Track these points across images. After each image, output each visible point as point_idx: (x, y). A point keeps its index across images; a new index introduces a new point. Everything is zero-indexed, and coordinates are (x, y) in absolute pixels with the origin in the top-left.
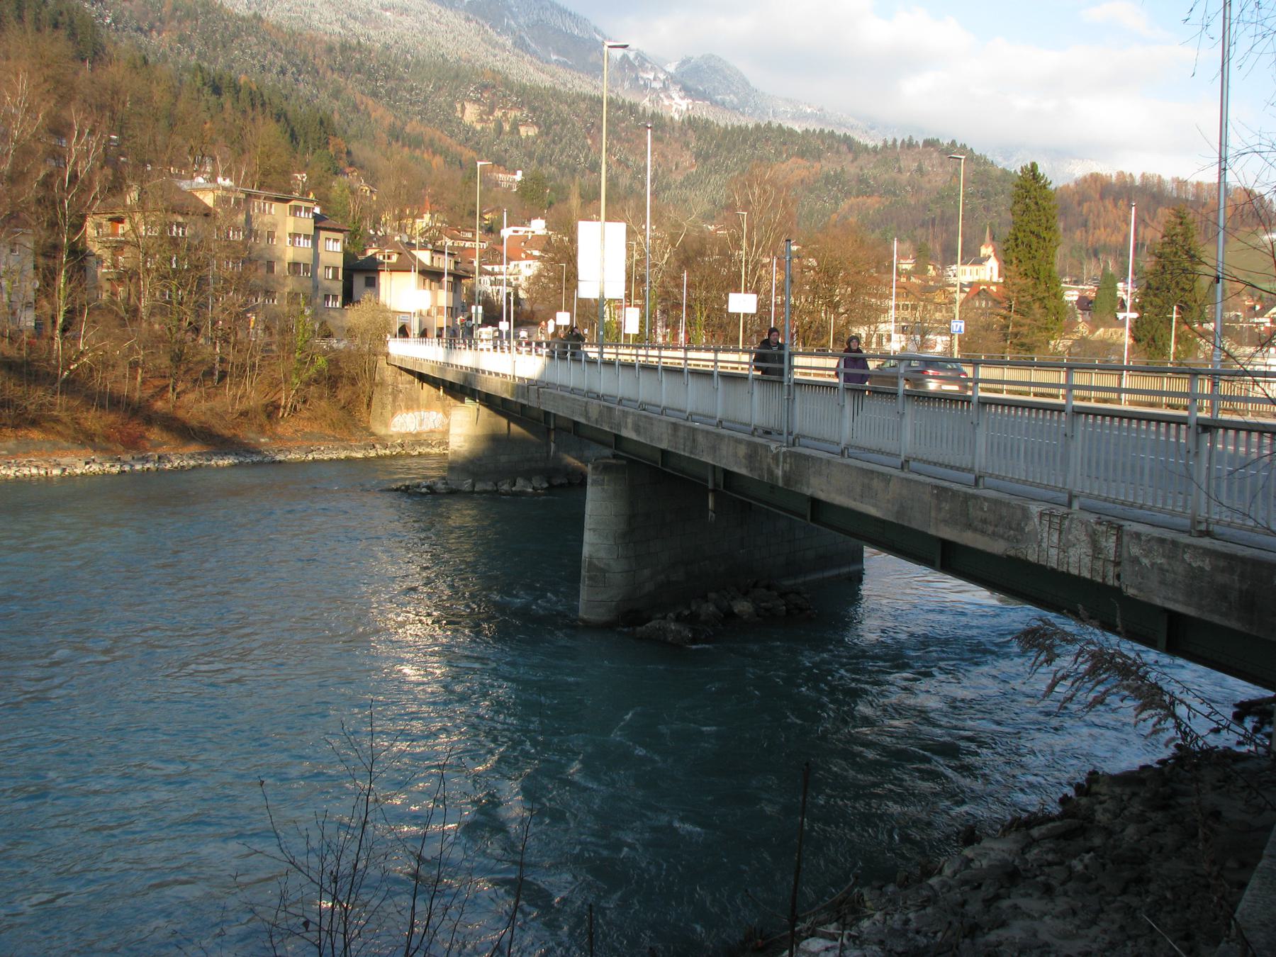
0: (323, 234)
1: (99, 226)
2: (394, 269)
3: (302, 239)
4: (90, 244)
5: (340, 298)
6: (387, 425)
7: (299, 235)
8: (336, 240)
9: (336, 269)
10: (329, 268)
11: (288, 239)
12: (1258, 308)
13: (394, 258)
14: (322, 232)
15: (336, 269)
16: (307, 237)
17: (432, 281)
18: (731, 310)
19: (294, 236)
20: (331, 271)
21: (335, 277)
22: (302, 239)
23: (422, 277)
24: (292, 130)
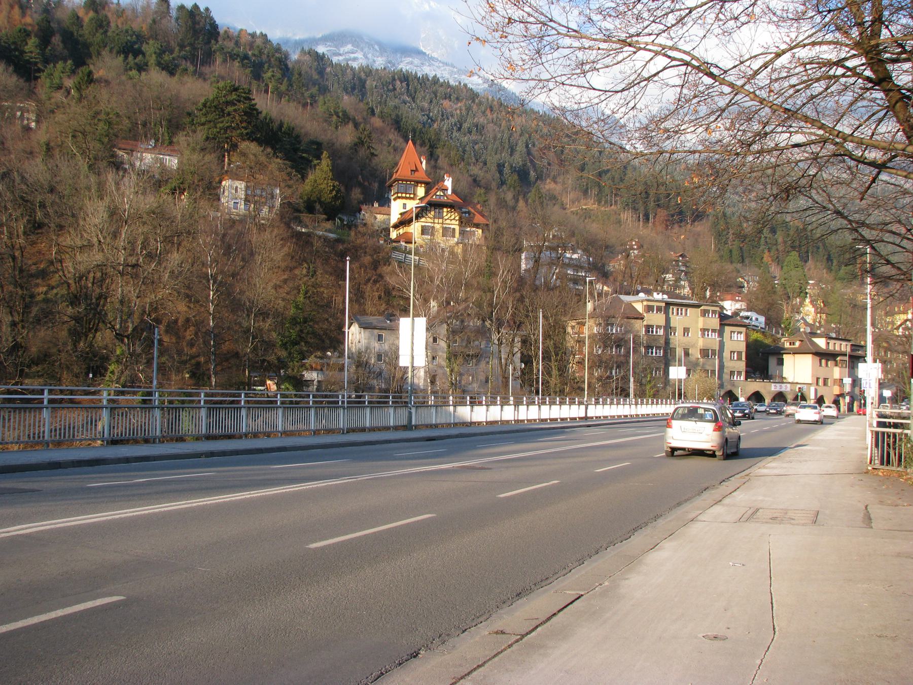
0: (728, 329)
1: (573, 327)
2: (796, 352)
3: (710, 333)
4: (108, 307)
5: (743, 374)
6: (131, 152)
7: (708, 330)
8: (741, 333)
9: (739, 353)
10: (734, 352)
11: (700, 333)
12: (885, 345)
13: (797, 344)
14: (726, 328)
15: (739, 353)
16: (714, 331)
17: (827, 361)
18: (860, 364)
19: (704, 330)
20: (736, 354)
21: (739, 358)
22: (710, 333)
23: (817, 359)
24: (829, 255)
